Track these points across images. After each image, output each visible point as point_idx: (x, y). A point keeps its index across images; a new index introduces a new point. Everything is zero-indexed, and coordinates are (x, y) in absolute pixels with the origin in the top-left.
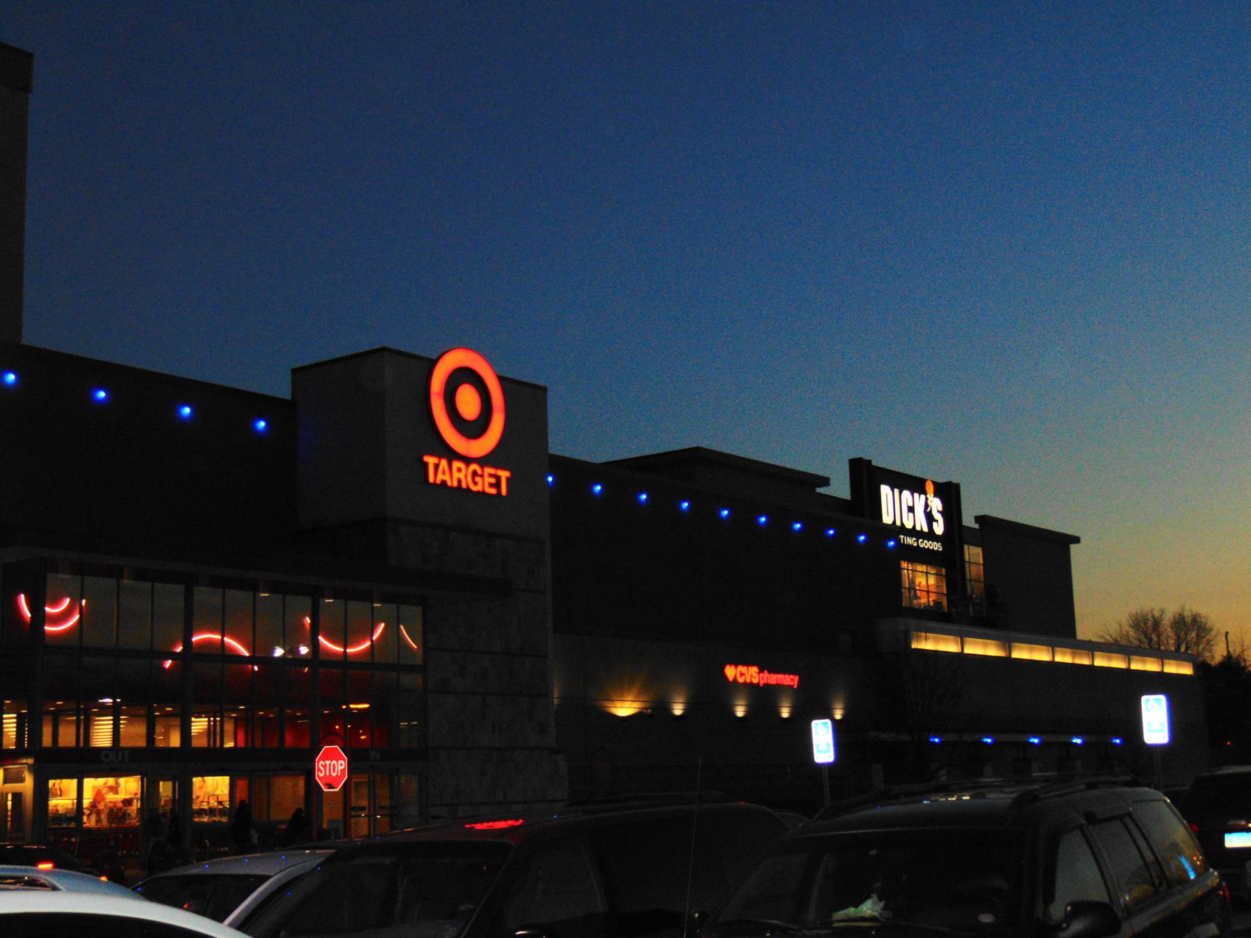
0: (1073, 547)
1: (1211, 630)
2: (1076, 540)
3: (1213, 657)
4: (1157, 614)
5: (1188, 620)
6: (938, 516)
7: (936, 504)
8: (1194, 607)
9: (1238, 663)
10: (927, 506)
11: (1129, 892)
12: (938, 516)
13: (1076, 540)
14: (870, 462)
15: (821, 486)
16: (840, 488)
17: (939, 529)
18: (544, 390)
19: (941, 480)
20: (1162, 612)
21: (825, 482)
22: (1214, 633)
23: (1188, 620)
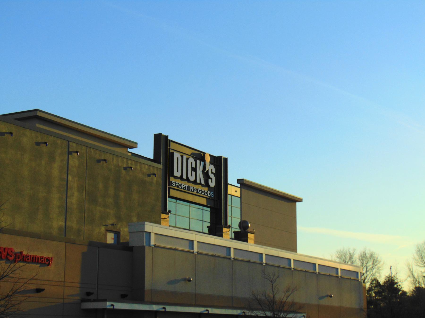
0: (297, 203)
1: (380, 262)
2: (300, 200)
3: (380, 276)
4: (351, 252)
5: (368, 255)
6: (212, 176)
7: (210, 168)
8: (370, 249)
9: (394, 280)
10: (204, 168)
11: (380, 305)
12: (212, 176)
13: (300, 200)
14: (167, 137)
15: (130, 148)
16: (146, 150)
17: (212, 184)
18: (293, 201)
19: (217, 155)
20: (355, 250)
21: (134, 145)
22: (381, 263)
23: (368, 255)
